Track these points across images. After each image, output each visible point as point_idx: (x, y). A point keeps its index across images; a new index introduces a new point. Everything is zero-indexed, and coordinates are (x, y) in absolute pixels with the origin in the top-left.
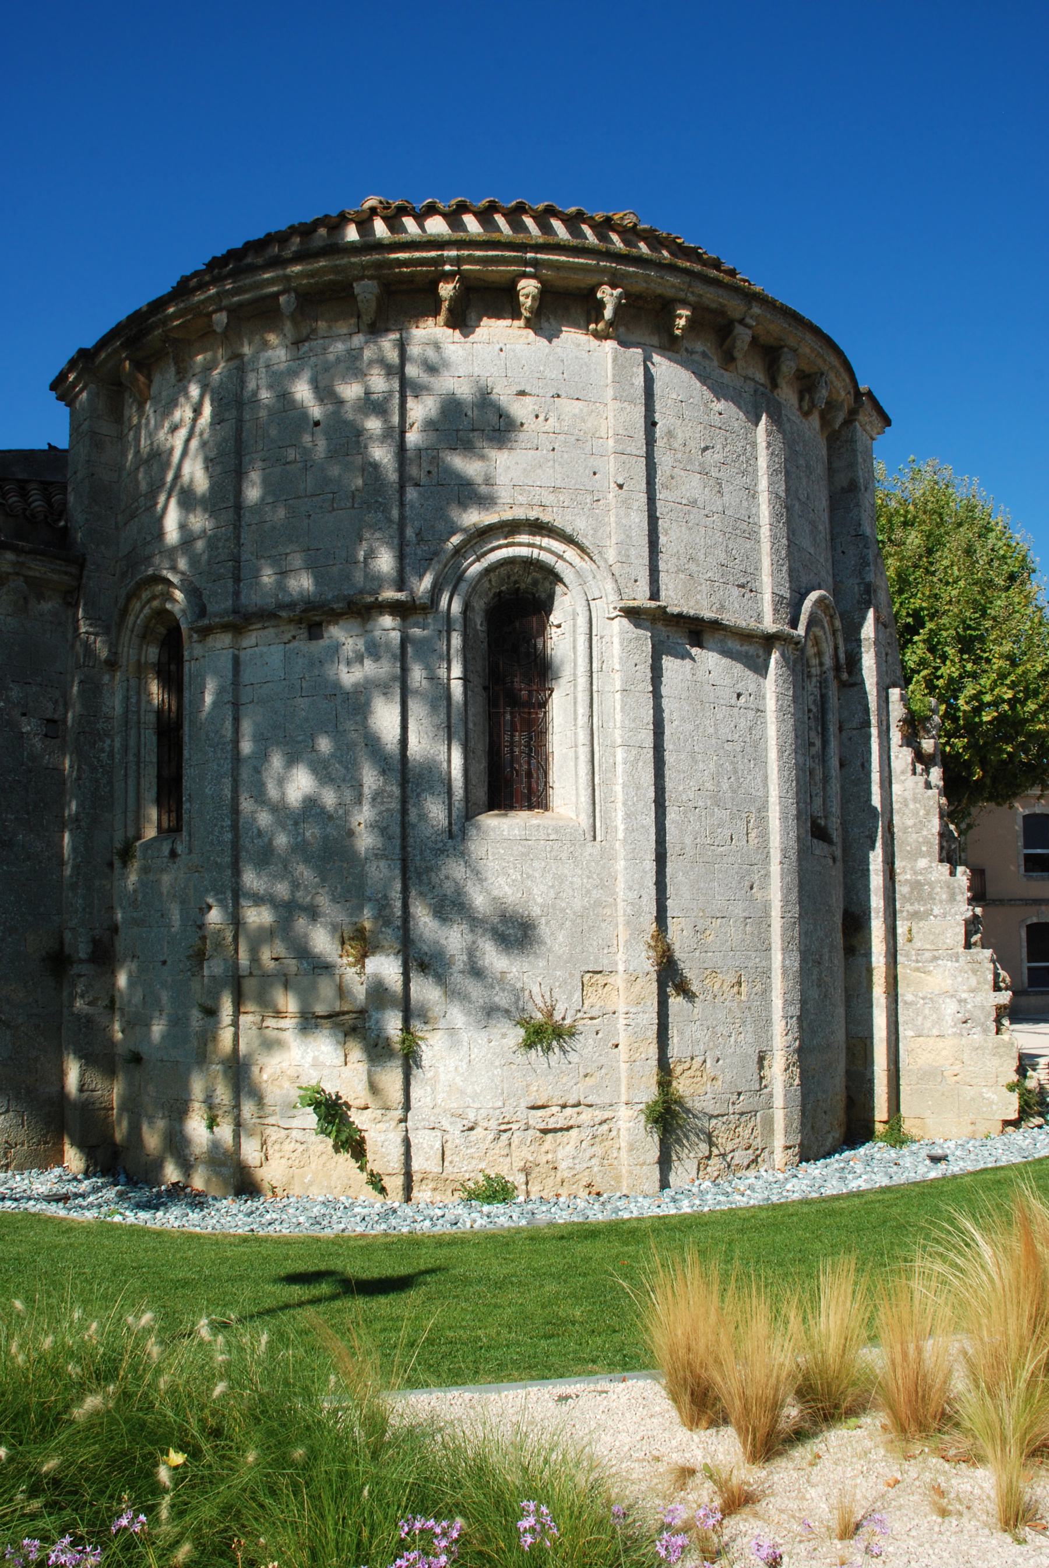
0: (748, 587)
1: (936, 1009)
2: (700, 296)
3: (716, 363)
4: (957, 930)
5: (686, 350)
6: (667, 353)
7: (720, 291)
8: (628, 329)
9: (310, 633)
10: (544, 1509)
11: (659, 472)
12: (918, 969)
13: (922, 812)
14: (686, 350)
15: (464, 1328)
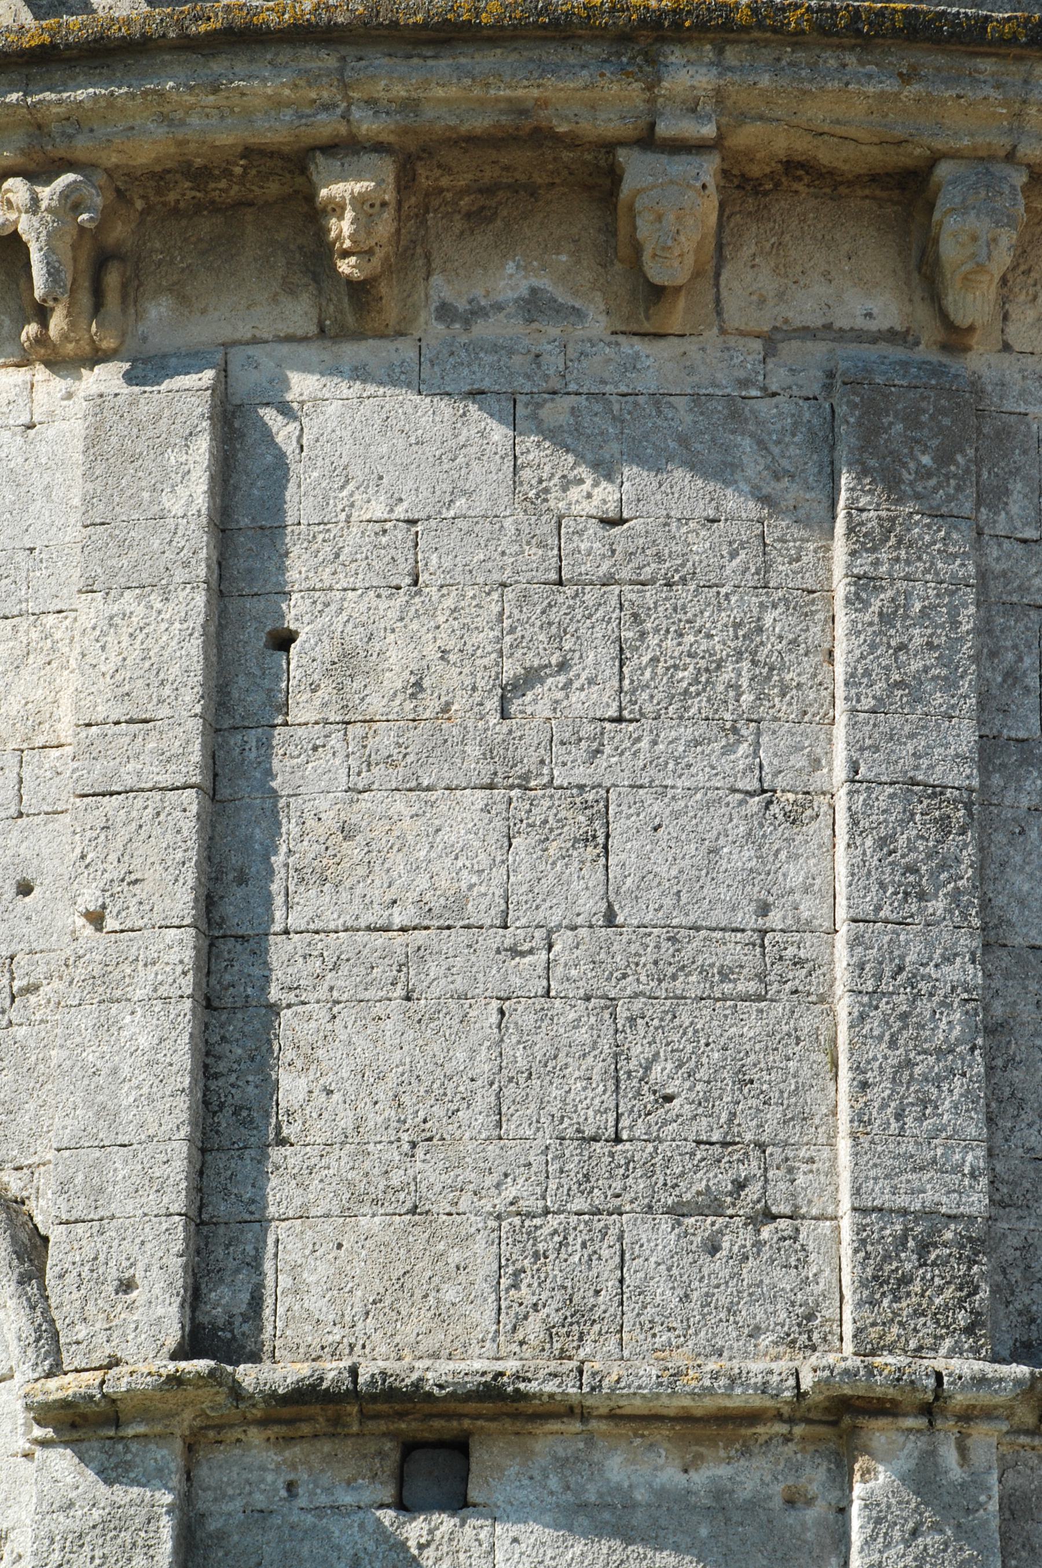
0: (739, 1204)
2: (410, 106)
5: (445, 312)
6: (352, 352)
7: (487, 60)
8: (183, 299)
9: (401, 1480)
11: (290, 827)
14: (445, 312)
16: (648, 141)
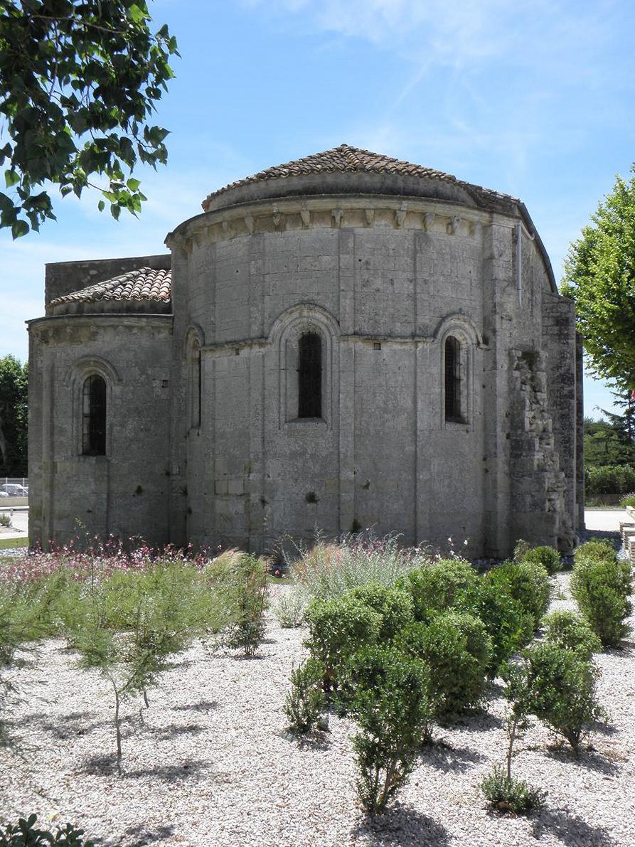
1: (523, 500)
3: (392, 228)
4: (31, 457)
5: (376, 225)
10: (349, 715)
12: (517, 481)
13: (520, 408)
15: (525, 839)
16: (400, 210)
